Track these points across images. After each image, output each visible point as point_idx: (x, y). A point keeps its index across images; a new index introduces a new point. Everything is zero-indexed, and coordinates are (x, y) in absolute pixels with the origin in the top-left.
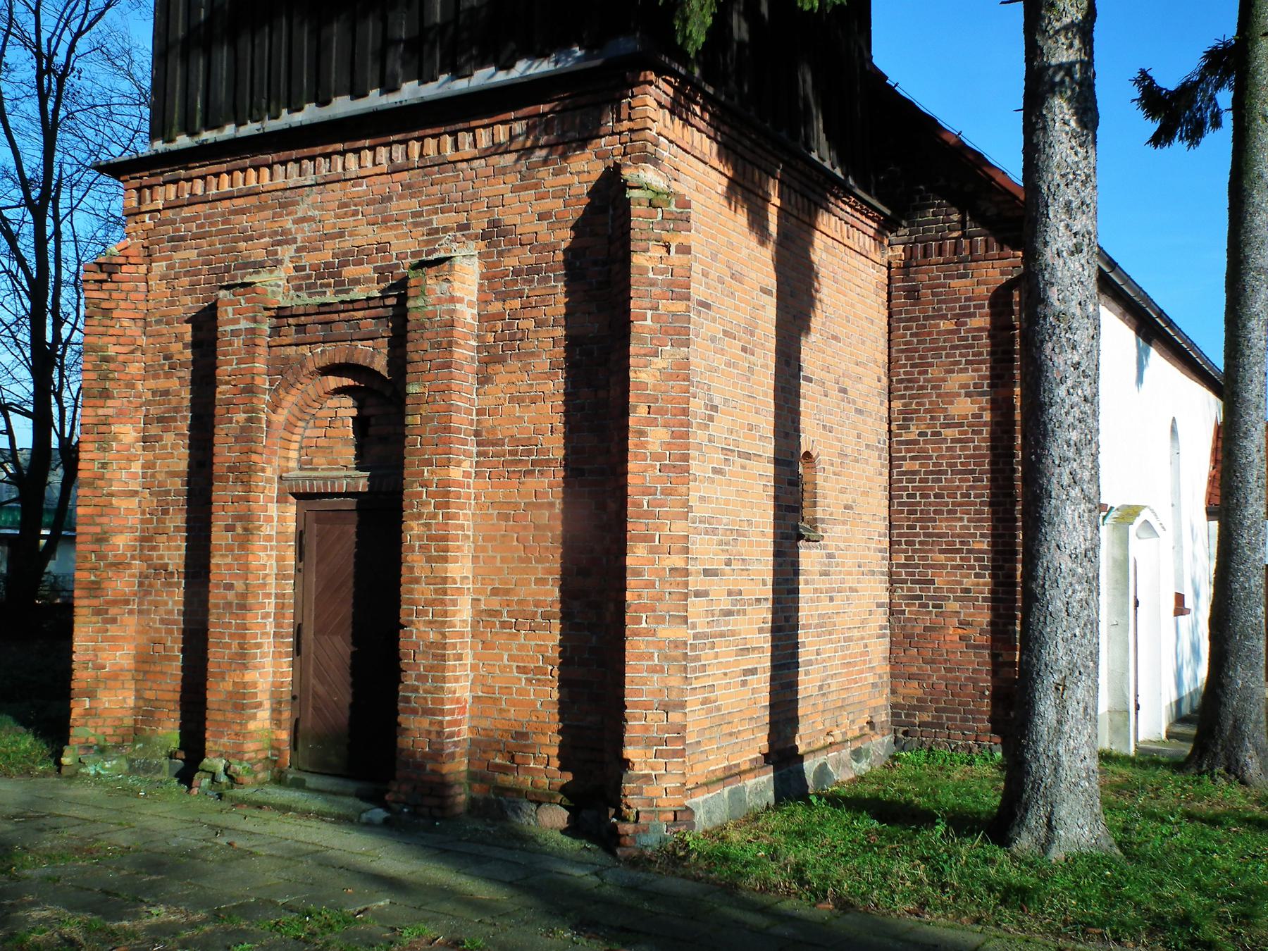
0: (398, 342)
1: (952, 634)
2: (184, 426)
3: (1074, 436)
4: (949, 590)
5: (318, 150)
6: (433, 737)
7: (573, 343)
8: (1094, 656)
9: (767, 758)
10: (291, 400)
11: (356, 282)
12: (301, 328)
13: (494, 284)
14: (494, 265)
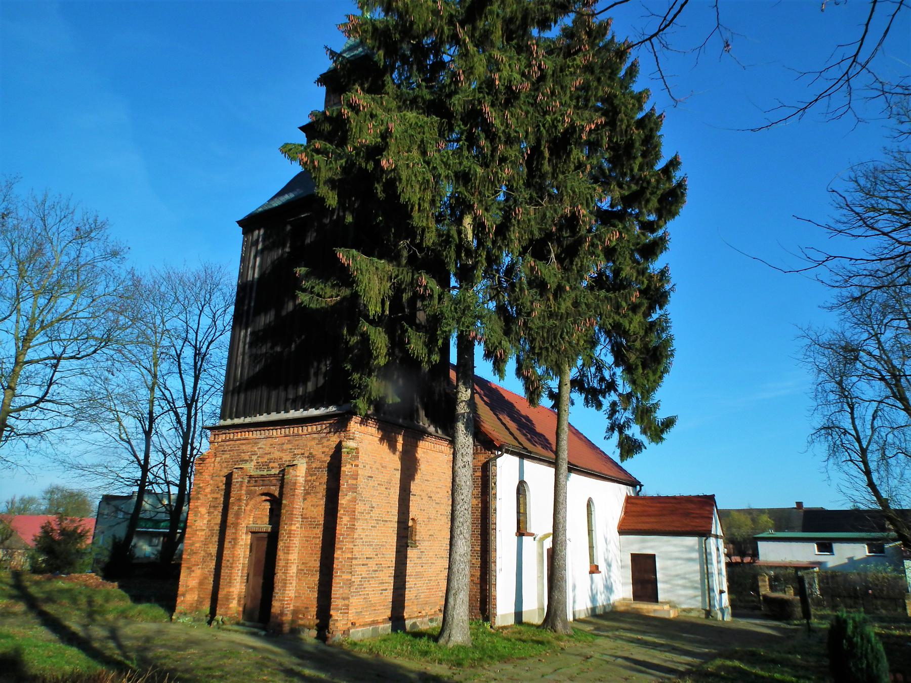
0: (282, 487)
2: (220, 509)
3: (461, 520)
9: (390, 619)
10: (252, 503)
11: (273, 468)
12: (256, 481)
13: (310, 472)
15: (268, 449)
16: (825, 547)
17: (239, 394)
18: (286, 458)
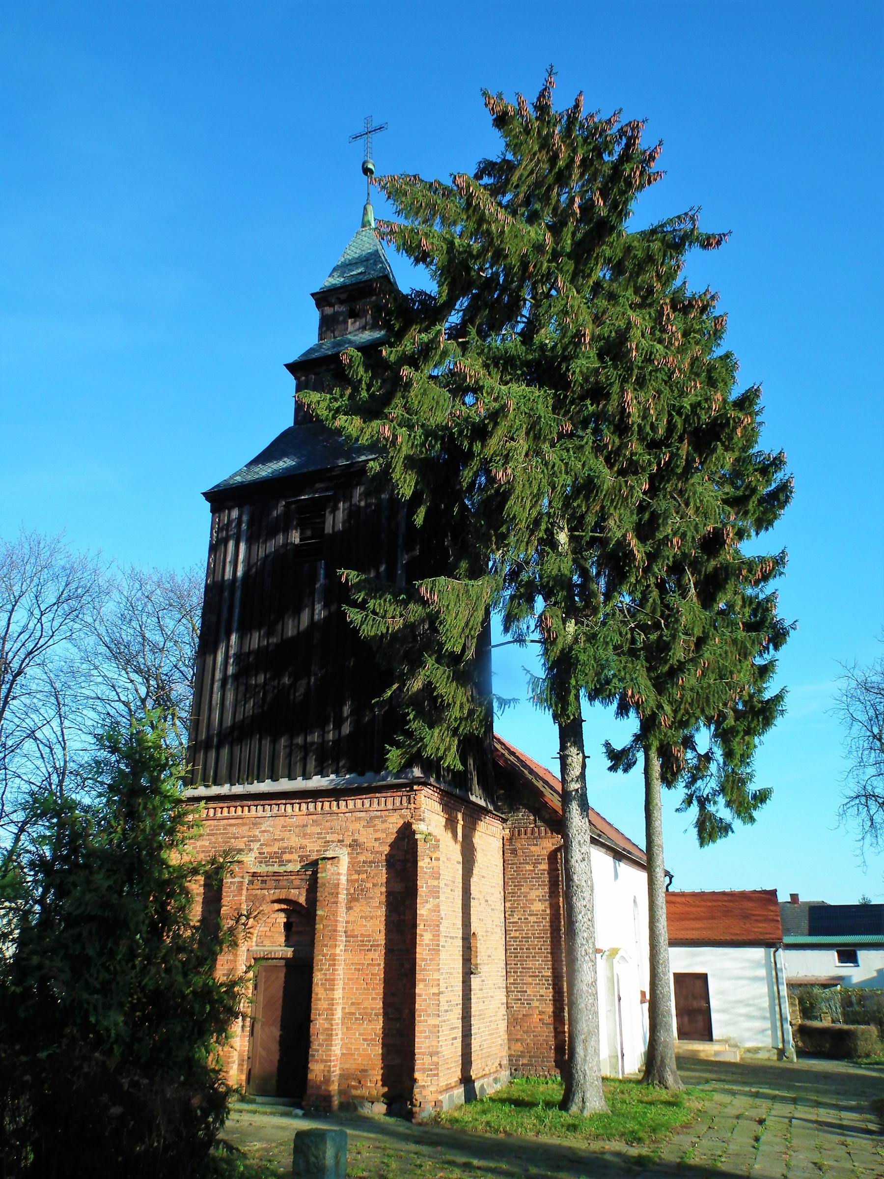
1: (536, 1018)
3: (585, 935)
4: (534, 996)
5: (274, 802)
6: (326, 1073)
7: (389, 894)
8: (597, 1027)
11: (289, 861)
13: (355, 868)
14: (354, 858)
15: (278, 834)
16: (848, 955)
17: (218, 748)
18: (313, 848)
